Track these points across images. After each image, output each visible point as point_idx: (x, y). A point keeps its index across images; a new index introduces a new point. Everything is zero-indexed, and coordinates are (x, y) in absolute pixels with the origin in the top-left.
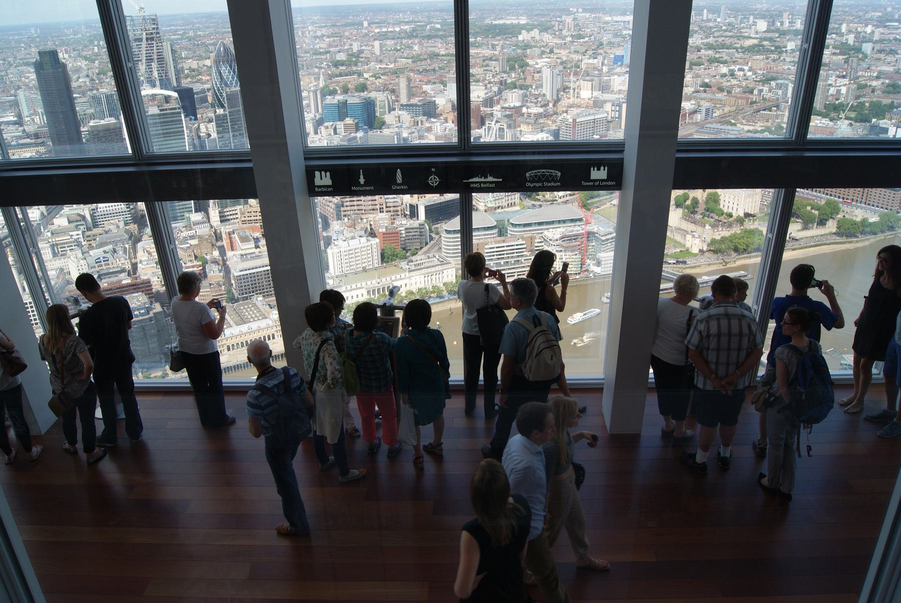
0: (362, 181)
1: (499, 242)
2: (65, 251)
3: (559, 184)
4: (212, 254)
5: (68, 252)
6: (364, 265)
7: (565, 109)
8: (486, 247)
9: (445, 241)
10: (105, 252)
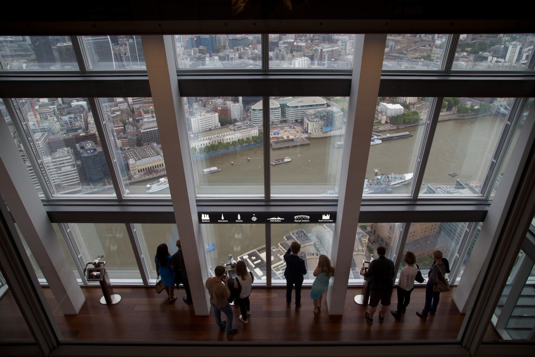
0: (223, 218)
2: (47, 117)
3: (309, 221)
4: (129, 120)
6: (210, 127)
7: (317, 44)
10: (70, 118)
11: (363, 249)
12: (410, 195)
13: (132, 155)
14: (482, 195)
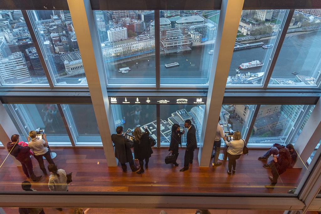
0: (126, 100)
1: (171, 30)
3: (187, 103)
4: (63, 32)
5: (4, 30)
6: (121, 38)
8: (167, 32)
9: (151, 31)
11: (226, 122)
12: (261, 85)
13: (66, 58)
14: (317, 86)
